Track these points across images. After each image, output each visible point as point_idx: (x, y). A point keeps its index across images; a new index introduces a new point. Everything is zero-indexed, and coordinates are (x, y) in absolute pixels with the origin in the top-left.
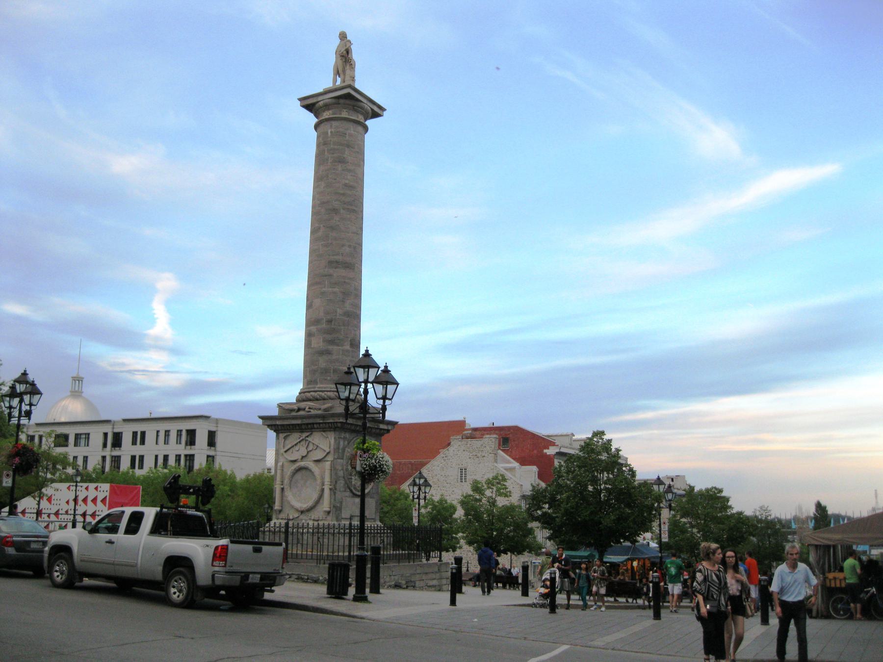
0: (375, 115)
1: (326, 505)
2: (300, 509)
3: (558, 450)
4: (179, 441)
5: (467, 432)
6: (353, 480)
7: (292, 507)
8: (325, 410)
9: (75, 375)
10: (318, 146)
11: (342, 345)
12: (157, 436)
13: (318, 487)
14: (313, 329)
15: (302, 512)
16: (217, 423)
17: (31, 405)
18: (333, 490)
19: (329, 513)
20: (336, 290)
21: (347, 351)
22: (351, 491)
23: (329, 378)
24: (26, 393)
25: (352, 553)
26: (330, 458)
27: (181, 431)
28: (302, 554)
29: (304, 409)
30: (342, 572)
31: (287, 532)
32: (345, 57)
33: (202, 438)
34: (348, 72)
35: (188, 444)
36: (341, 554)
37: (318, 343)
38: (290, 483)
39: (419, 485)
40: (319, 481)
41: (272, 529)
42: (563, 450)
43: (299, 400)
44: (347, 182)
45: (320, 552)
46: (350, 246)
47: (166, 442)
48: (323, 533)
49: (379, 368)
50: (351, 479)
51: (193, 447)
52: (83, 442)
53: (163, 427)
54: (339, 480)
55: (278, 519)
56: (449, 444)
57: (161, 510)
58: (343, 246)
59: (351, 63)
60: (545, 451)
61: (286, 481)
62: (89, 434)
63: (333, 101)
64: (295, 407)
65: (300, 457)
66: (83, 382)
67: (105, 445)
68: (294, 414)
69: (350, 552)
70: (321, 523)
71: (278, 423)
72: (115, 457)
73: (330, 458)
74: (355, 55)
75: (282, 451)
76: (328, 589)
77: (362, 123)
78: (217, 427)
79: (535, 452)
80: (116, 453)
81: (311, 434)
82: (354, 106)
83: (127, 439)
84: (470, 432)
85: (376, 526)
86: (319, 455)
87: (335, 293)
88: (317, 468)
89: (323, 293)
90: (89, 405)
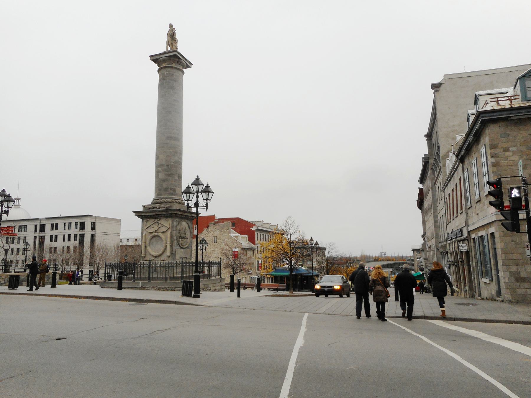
0: (188, 67)
1: (168, 253)
2: (155, 256)
3: (257, 228)
4: (76, 228)
5: (216, 220)
6: (181, 241)
7: (151, 254)
8: (167, 208)
10: (160, 80)
12: (65, 225)
13: (164, 245)
14: (160, 169)
15: (156, 257)
16: (96, 219)
17: (8, 207)
18: (171, 246)
19: (169, 256)
22: (180, 246)
24: (5, 201)
25: (151, 276)
26: (170, 230)
27: (77, 223)
29: (156, 208)
30: (12, 284)
31: (150, 267)
32: (172, 37)
33: (88, 226)
34: (174, 44)
35: (81, 229)
36: (187, 275)
37: (162, 176)
38: (150, 244)
39: (203, 244)
40: (164, 242)
41: (142, 266)
42: (259, 228)
43: (153, 203)
45: (190, 274)
49: (203, 185)
50: (180, 240)
51: (83, 230)
52: (23, 230)
53: (67, 221)
54: (174, 241)
55: (143, 261)
56: (208, 226)
59: (176, 40)
60: (251, 228)
61: (147, 242)
62: (27, 226)
63: (167, 58)
64: (152, 207)
65: (155, 231)
66: (21, 200)
67: (36, 231)
68: (151, 210)
69: (182, 275)
70: (167, 261)
71: (143, 214)
72: (42, 236)
73: (170, 230)
74: (178, 36)
75: (145, 228)
76: (182, 293)
77: (182, 70)
78: (96, 220)
79: (247, 229)
80: (42, 234)
83: (48, 227)
84: (217, 220)
86: (164, 229)
88: (163, 236)
89: (164, 152)
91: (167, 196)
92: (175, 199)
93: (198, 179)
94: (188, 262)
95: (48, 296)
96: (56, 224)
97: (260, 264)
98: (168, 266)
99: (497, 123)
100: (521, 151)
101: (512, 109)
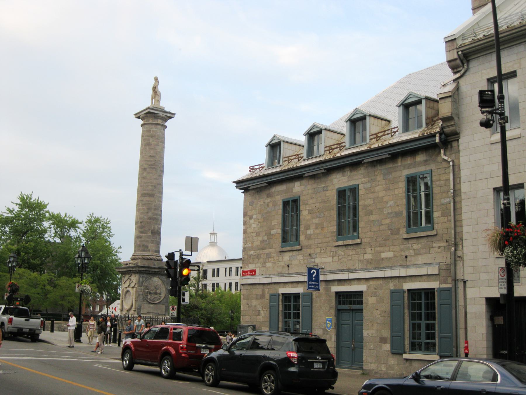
4: (237, 274)
8: (134, 264)
9: (212, 232)
11: (147, 233)
12: (226, 271)
20: (145, 207)
21: (150, 236)
22: (147, 301)
23: (140, 249)
41: (163, 320)
44: (151, 154)
46: (152, 186)
47: (230, 275)
53: (228, 265)
57: (5, 306)
58: (148, 186)
63: (145, 115)
72: (204, 284)
81: (131, 275)
82: (155, 116)
83: (210, 273)
85: (166, 318)
87: (144, 209)
90: (221, 250)
91: (139, 253)
92: (146, 255)
94: (153, 318)
96: (217, 269)
99: (282, 184)
100: (258, 219)
101: (282, 171)
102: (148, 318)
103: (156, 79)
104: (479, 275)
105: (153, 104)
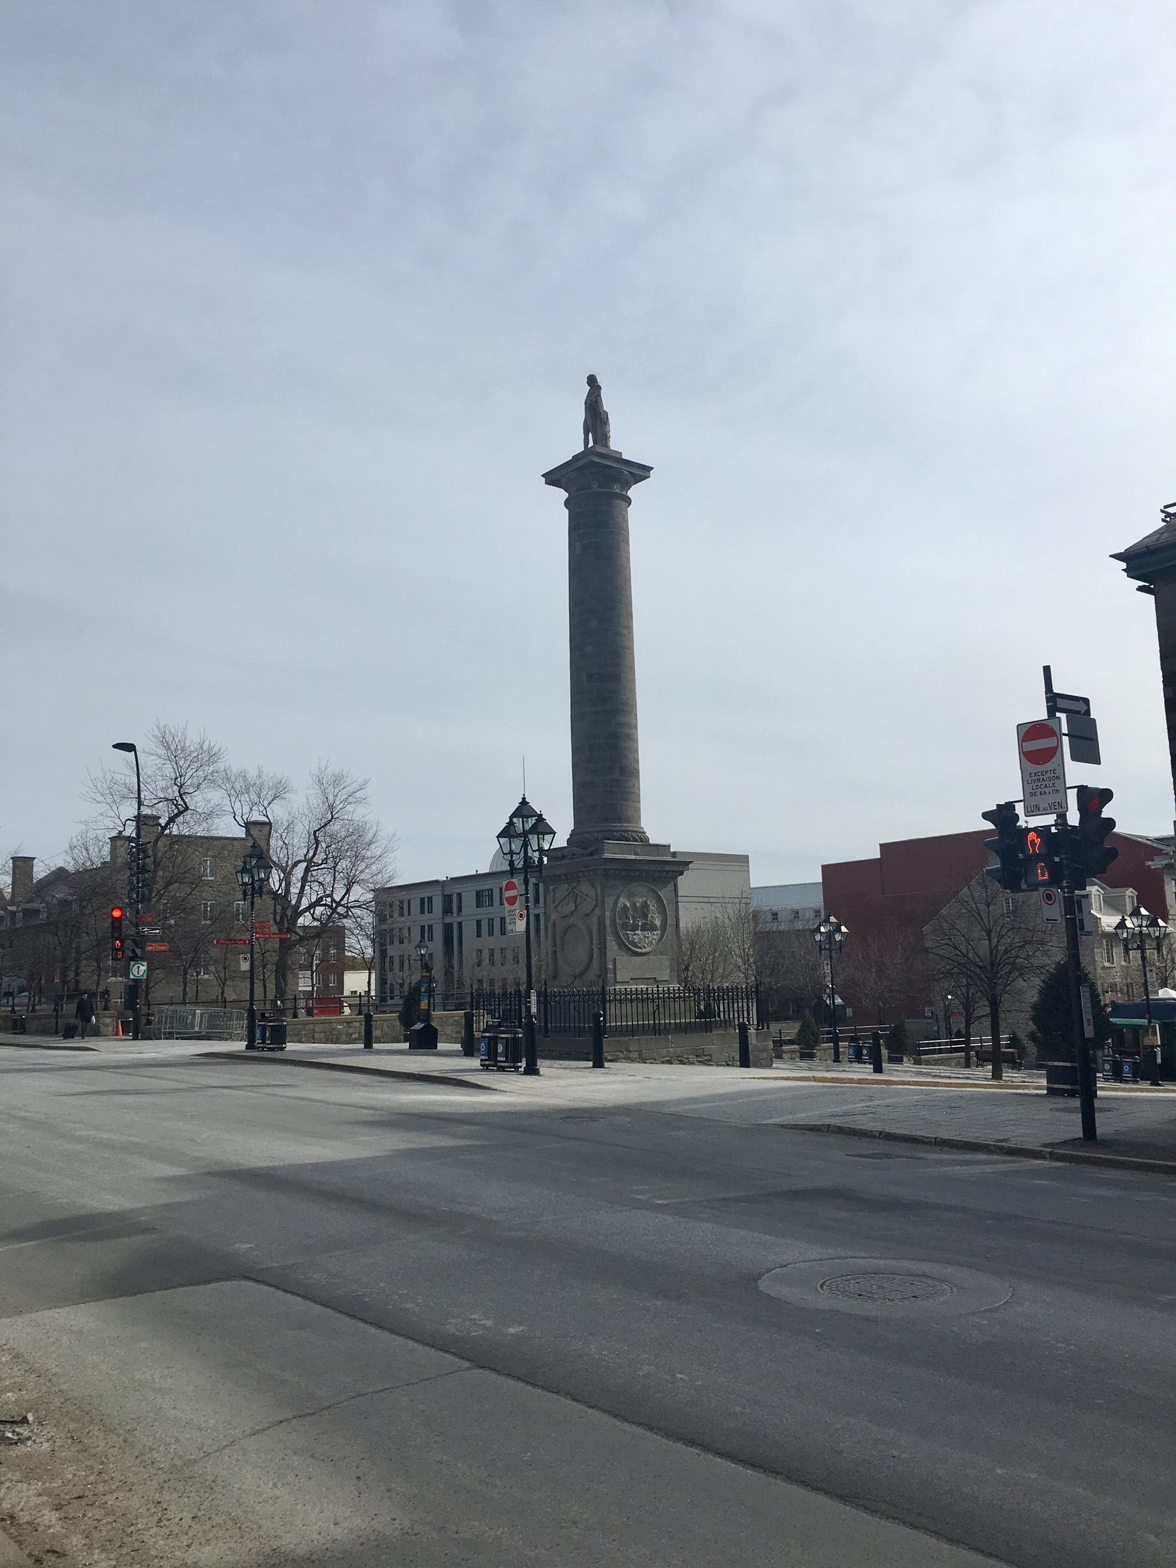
28: (579, 1026)
36: (683, 1021)
48: (664, 998)
83: (469, 900)
93: (524, 802)
95: (457, 1070)
97: (645, 994)
98: (621, 1000)
102: (626, 994)
103: (592, 380)
104: (681, 896)
105: (591, 444)
